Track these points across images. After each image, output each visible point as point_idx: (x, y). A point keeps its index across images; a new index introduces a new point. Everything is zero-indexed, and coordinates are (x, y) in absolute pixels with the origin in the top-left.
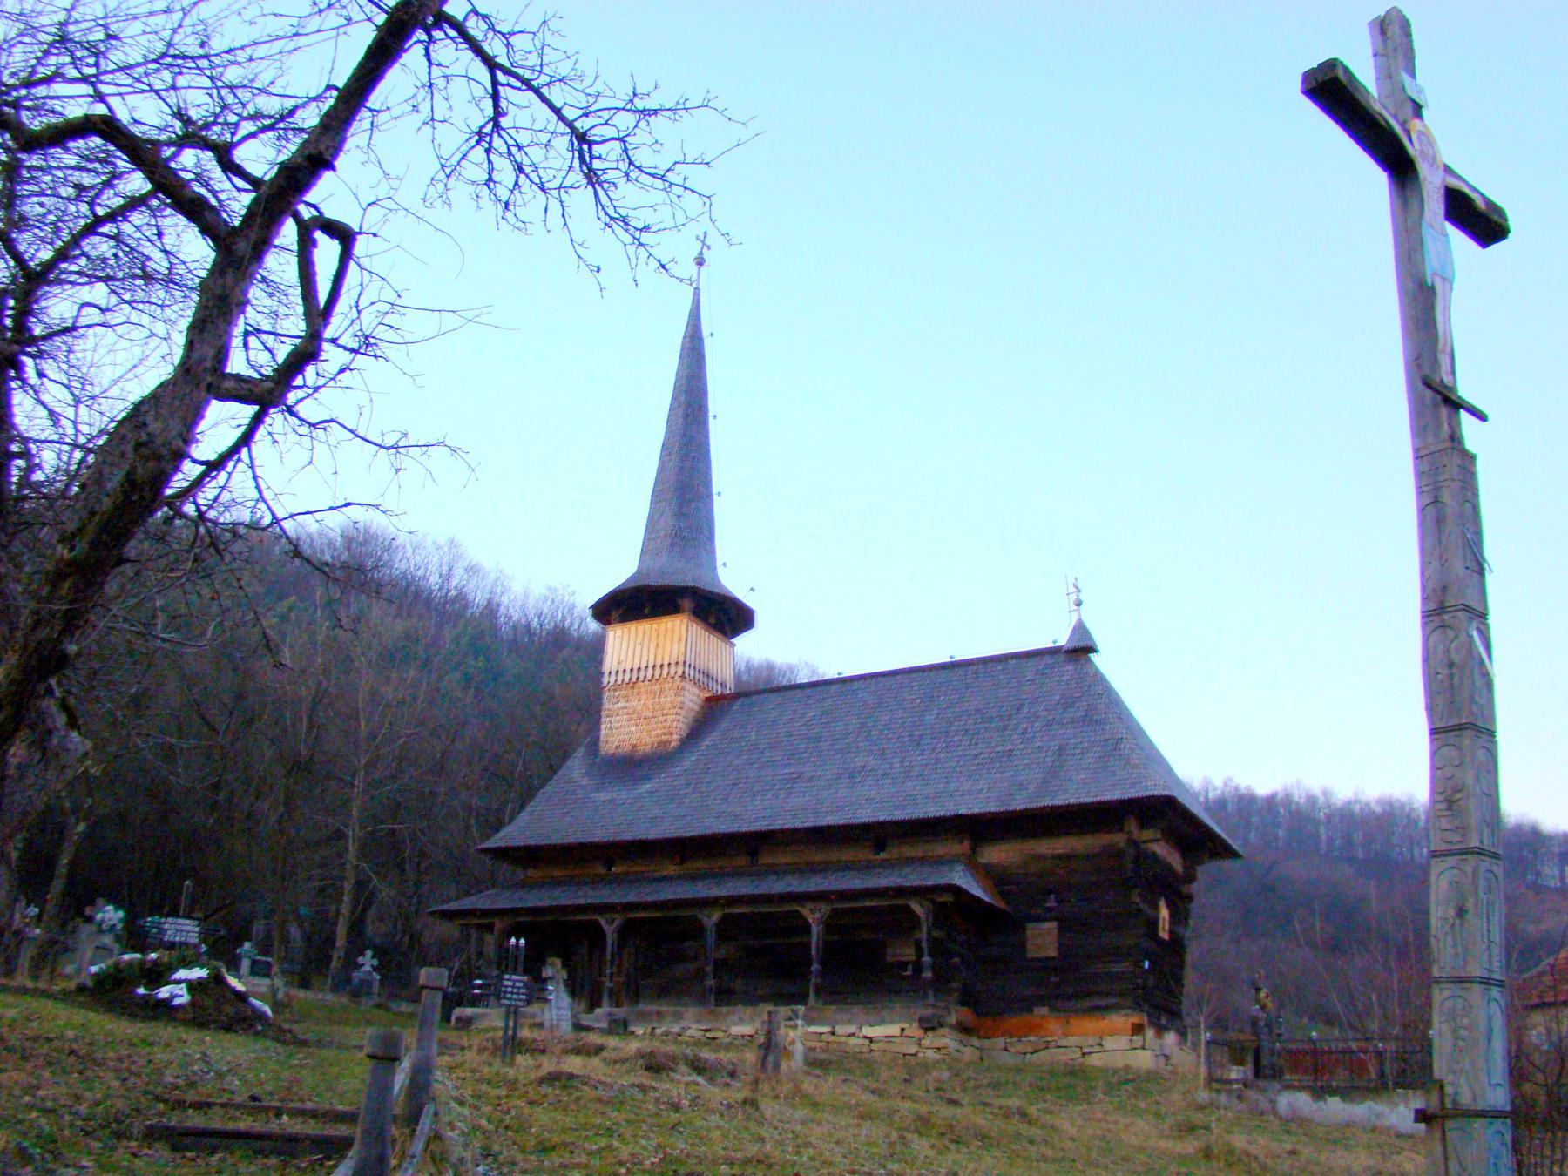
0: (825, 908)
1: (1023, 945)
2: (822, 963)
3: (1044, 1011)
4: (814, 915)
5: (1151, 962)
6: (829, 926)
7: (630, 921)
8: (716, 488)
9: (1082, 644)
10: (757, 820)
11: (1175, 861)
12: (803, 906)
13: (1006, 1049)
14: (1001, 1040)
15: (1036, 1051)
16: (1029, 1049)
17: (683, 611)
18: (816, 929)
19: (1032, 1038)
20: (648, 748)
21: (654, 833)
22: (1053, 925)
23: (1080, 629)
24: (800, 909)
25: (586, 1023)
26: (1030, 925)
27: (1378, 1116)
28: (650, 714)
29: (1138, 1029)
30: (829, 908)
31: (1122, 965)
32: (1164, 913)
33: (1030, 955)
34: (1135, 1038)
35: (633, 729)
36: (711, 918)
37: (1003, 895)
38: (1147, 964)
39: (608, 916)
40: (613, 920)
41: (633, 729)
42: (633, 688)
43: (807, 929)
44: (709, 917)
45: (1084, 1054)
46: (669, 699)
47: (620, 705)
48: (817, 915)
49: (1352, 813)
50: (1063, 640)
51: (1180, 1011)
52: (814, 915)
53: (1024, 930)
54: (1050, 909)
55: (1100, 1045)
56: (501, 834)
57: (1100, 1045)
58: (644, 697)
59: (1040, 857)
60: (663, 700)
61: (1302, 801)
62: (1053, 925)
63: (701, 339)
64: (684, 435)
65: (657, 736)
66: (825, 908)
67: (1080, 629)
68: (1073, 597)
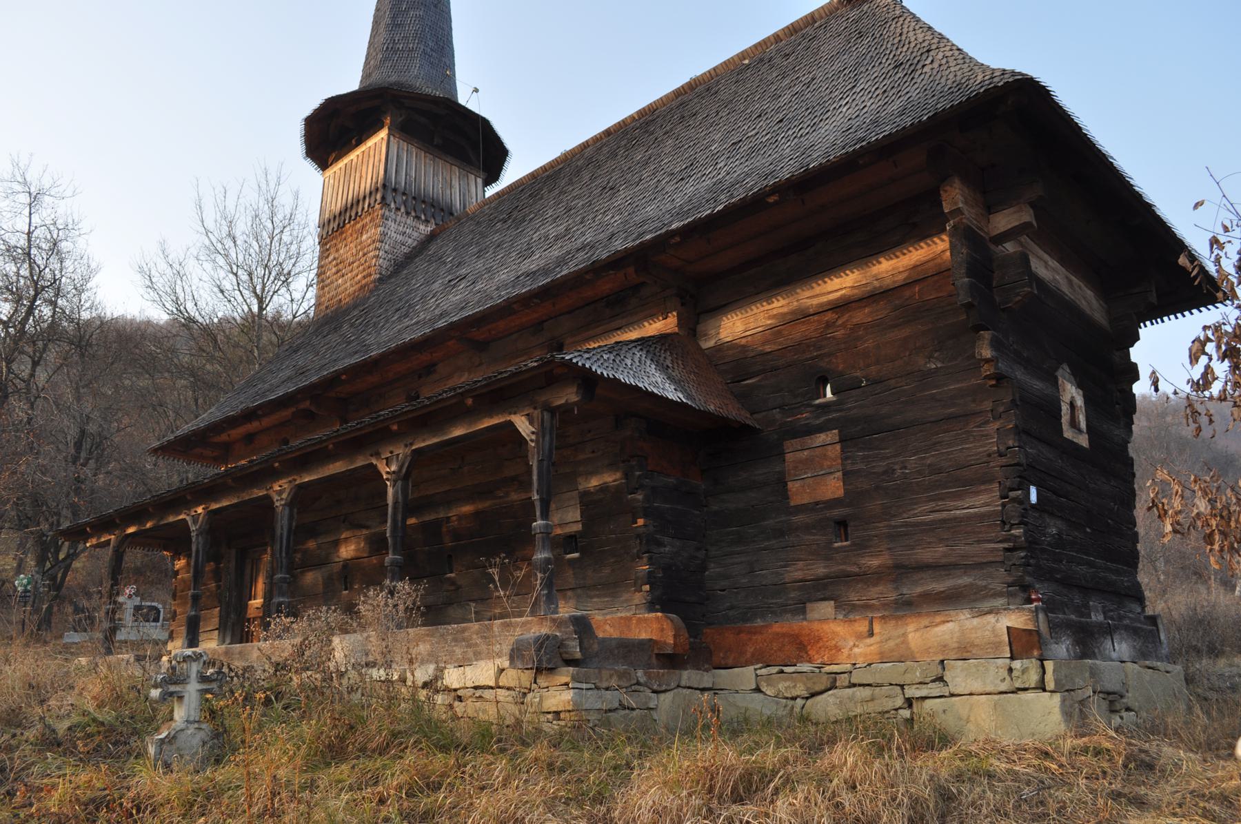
3: (827, 608)
5: (1089, 527)
6: (404, 477)
7: (301, 487)
11: (1087, 299)
13: (758, 690)
14: (749, 671)
15: (813, 695)
16: (800, 690)
19: (805, 667)
22: (831, 436)
25: (764, 690)
26: (790, 445)
29: (1021, 644)
32: (1071, 392)
33: (796, 501)
34: (1017, 664)
37: (743, 397)
38: (1088, 530)
45: (909, 702)
47: (331, 258)
51: (1138, 586)
53: (782, 454)
57: (940, 679)
62: (831, 436)
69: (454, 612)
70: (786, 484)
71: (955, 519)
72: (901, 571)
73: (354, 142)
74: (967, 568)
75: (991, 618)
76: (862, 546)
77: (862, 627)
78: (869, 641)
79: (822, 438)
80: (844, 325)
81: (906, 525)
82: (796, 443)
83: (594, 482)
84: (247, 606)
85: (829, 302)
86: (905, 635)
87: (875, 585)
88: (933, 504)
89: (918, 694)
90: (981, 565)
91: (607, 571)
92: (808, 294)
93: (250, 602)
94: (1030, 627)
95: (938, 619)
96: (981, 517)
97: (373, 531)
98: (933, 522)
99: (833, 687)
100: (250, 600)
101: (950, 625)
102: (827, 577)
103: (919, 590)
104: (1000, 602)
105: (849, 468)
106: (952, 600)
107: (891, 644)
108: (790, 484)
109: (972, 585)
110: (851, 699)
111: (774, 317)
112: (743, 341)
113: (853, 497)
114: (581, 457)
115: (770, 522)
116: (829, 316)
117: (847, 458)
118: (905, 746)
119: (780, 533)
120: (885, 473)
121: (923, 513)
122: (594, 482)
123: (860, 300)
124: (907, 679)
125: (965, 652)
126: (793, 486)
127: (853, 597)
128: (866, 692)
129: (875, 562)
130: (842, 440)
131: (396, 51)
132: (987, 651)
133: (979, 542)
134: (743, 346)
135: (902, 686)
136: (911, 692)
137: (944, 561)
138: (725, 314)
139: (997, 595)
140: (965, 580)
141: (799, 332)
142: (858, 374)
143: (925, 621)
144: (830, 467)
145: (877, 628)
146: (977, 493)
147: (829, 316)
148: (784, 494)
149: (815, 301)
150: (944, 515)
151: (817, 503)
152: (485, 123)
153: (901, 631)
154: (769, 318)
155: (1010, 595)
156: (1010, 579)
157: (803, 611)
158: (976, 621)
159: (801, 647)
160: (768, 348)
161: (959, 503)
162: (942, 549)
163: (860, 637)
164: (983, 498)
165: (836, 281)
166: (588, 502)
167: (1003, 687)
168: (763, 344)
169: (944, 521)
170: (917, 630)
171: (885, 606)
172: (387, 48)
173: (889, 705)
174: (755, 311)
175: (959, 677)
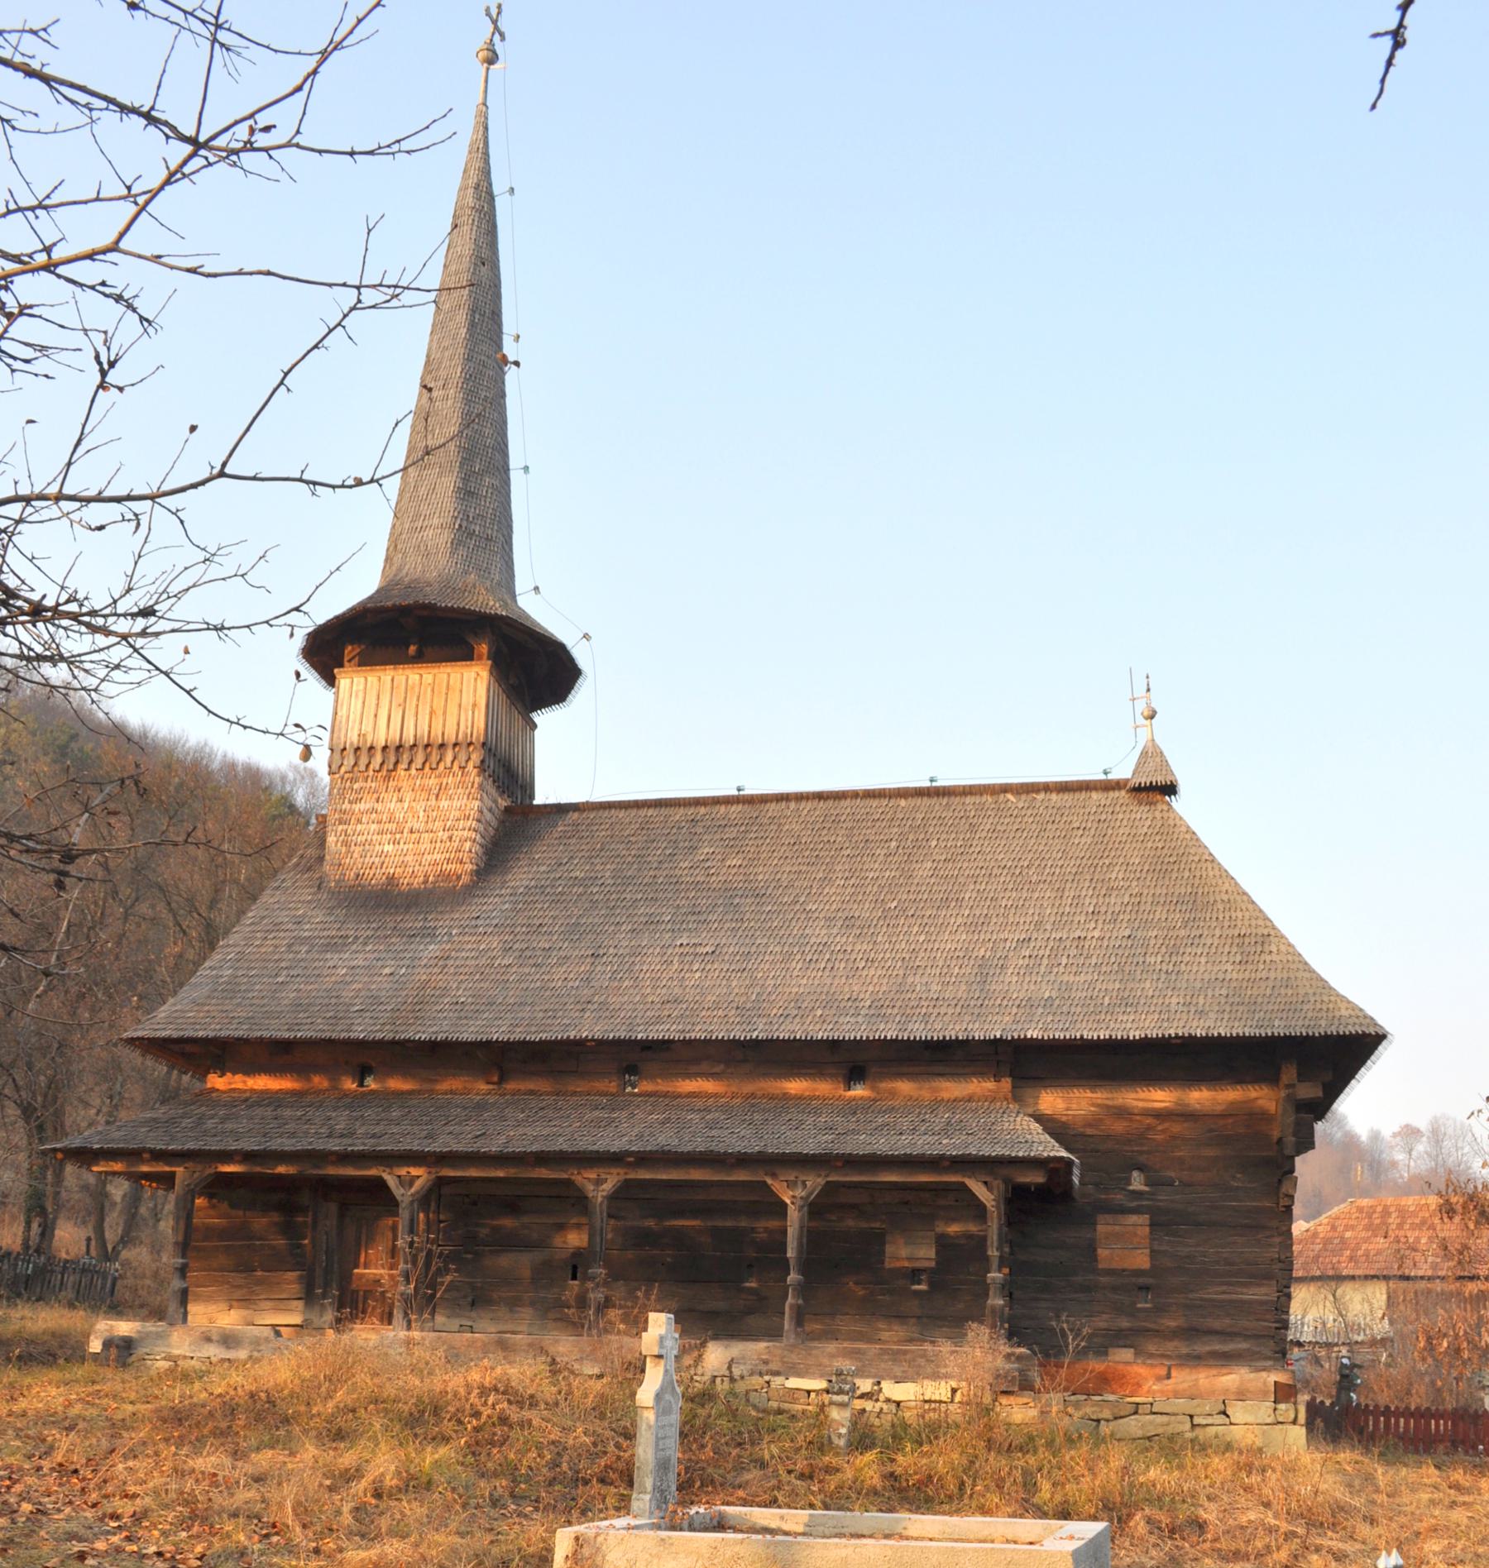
0: (814, 1182)
1: (1091, 1249)
2: (805, 1267)
3: (1126, 1354)
4: (793, 1194)
6: (815, 1209)
8: (516, 458)
9: (1160, 779)
10: (659, 1020)
12: (774, 1175)
17: (480, 658)
18: (793, 1215)
19: (1111, 1397)
20: (417, 882)
21: (469, 1032)
22: (1144, 1219)
23: (1151, 754)
24: (769, 1181)
26: (1101, 1218)
27: (650, 1427)
28: (421, 826)
30: (821, 1181)
31: (1256, 1290)
34: (1282, 1406)
35: (388, 848)
36: (600, 1186)
39: (403, 1171)
40: (412, 1180)
41: (388, 848)
42: (387, 778)
43: (781, 1209)
44: (599, 1182)
46: (456, 804)
47: (362, 806)
48: (800, 1192)
49: (209, 774)
50: (1124, 771)
52: (793, 1194)
53: (1095, 1224)
54: (1138, 1194)
55: (1224, 1413)
56: (163, 1012)
57: (1224, 1413)
58: (408, 797)
59: (1122, 1113)
60: (444, 804)
61: (216, 765)
62: (1144, 1219)
63: (491, 197)
64: (469, 359)
65: (436, 863)
66: (814, 1182)
67: (1151, 754)
68: (1141, 706)
69: (752, 1321)
70: (1095, 1250)
71: (1242, 1302)
72: (1191, 1333)
73: (412, 649)
74: (1246, 1337)
75: (1264, 1374)
76: (1159, 1310)
77: (1163, 1372)
78: (1166, 1382)
79: (1133, 1219)
80: (1163, 1131)
81: (1202, 1299)
82: (1109, 1218)
83: (954, 1229)
84: (351, 1274)
85: (1154, 1109)
86: (1196, 1380)
87: (1171, 1340)
88: (1224, 1288)
89: (1204, 1422)
90: (1257, 1337)
91: (961, 1306)
92: (1133, 1095)
93: (356, 1271)
94: (1291, 1382)
95: (1224, 1371)
96: (1262, 1303)
97: (629, 1224)
98: (1223, 1301)
99: (1136, 1413)
100: (357, 1266)
101: (1233, 1376)
102: (1130, 1329)
103: (1208, 1348)
104: (1270, 1363)
105: (1156, 1247)
106: (1227, 1359)
107: (1185, 1385)
108: (1100, 1251)
109: (1248, 1350)
110: (1151, 1423)
111: (1098, 1105)
112: (1064, 1119)
113: (1154, 1271)
114: (942, 1202)
115: (1079, 1279)
116: (1149, 1121)
117: (1154, 1239)
118: (1397, 1423)
119: (1086, 1289)
120: (1187, 1257)
121: (1215, 1293)
122: (954, 1229)
123: (1177, 1115)
124: (1198, 1411)
125: (1241, 1395)
126: (1102, 1253)
127: (1152, 1348)
128: (1165, 1419)
129: (1173, 1324)
130: (1151, 1225)
131: (471, 534)
132: (1261, 1395)
133: (1258, 1320)
134: (1064, 1123)
135: (1191, 1417)
136: (1197, 1420)
137: (1229, 1330)
138: (1046, 1087)
139: (1270, 1358)
140: (1244, 1345)
141: (1119, 1127)
142: (1173, 1174)
143: (1214, 1372)
144: (1139, 1243)
145: (1174, 1373)
146: (1259, 1285)
147: (1149, 1121)
148: (1094, 1257)
149: (1141, 1104)
150: (1234, 1297)
151: (1124, 1270)
152: (561, 647)
153: (1194, 1377)
154: (1093, 1105)
155: (1276, 1359)
156: (1277, 1349)
157: (1106, 1354)
158: (1252, 1375)
159: (1104, 1382)
160: (1089, 1131)
161: (1245, 1290)
162: (1228, 1321)
163: (1159, 1379)
164: (1263, 1290)
165: (1159, 1092)
166: (943, 1243)
167: (1269, 1420)
168: (1085, 1126)
169: (1231, 1301)
170: (1207, 1377)
171: (1179, 1357)
172: (460, 526)
173: (1180, 1428)
174: (1077, 1095)
175: (1238, 1412)
